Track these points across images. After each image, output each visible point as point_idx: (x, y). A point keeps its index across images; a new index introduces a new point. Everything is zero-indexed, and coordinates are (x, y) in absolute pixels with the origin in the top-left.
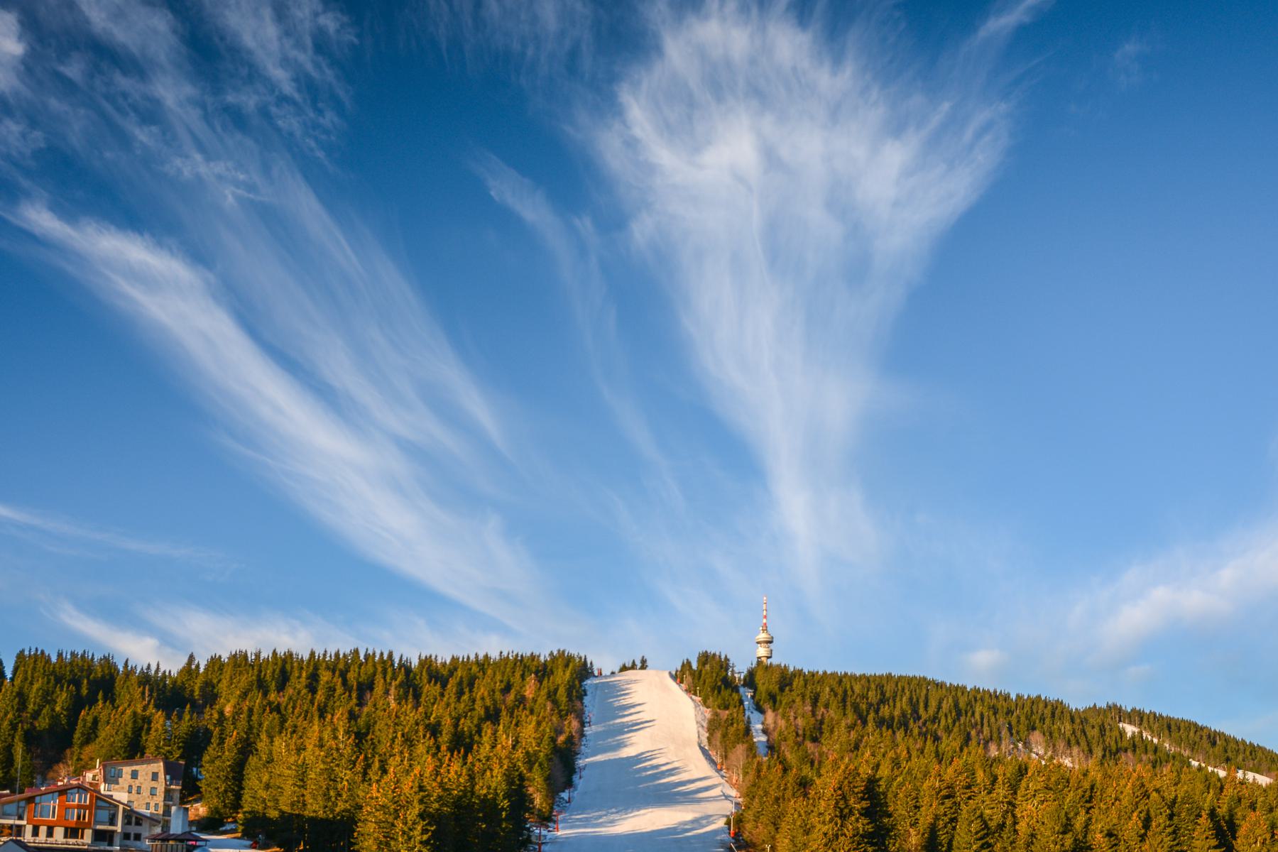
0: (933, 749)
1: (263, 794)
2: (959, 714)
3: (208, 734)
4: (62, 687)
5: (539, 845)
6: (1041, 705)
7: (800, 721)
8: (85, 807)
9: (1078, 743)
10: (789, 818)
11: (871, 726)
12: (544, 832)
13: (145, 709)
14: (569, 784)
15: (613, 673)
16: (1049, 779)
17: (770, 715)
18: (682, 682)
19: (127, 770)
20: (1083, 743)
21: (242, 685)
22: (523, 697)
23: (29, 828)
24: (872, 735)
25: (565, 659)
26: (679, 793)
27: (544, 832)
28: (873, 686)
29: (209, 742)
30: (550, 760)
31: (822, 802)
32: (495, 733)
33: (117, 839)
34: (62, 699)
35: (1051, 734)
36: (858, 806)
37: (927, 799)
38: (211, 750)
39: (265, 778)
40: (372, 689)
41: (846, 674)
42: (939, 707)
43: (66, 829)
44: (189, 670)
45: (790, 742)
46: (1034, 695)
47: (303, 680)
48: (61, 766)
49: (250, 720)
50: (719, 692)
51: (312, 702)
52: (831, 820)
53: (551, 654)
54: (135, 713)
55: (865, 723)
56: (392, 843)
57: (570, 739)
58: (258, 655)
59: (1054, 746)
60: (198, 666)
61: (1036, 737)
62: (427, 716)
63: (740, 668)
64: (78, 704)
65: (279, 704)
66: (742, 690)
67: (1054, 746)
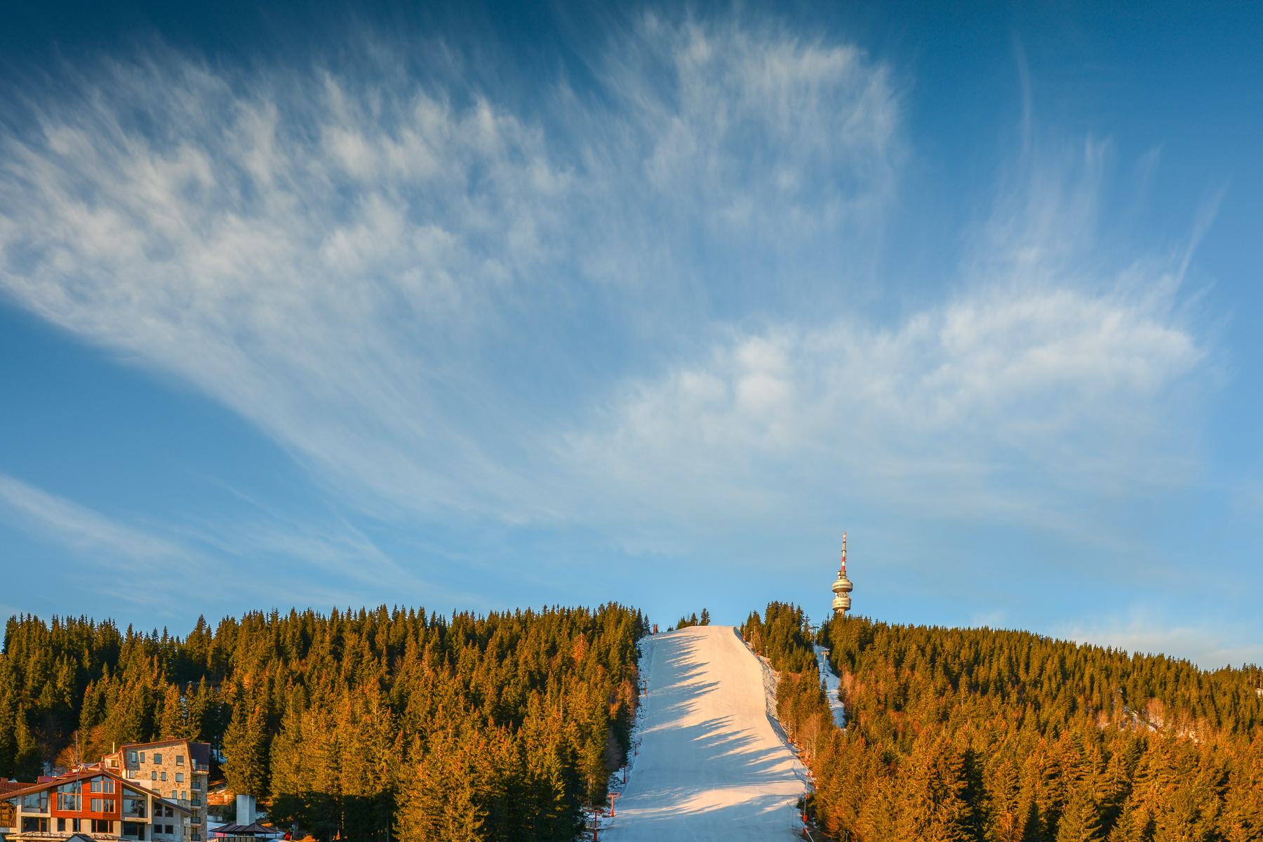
0: (1034, 718)
1: (293, 778)
2: (1065, 676)
3: (227, 710)
4: (62, 659)
5: (595, 832)
6: (1163, 667)
7: (881, 686)
8: (111, 797)
9: (1205, 713)
10: (872, 800)
11: (963, 689)
12: (599, 817)
13: (156, 682)
14: (623, 762)
15: (670, 630)
16: (1173, 756)
17: (848, 677)
18: (748, 640)
19: (149, 753)
20: (1212, 714)
21: (260, 652)
22: (570, 659)
23: (54, 823)
24: (964, 702)
25: (615, 613)
26: (761, 775)
27: (599, 817)
28: (967, 644)
29: (229, 720)
30: (602, 734)
31: (912, 782)
32: (542, 701)
33: (148, 832)
34: (64, 673)
35: (1173, 701)
36: (954, 787)
37: (1028, 779)
38: (233, 729)
39: (295, 760)
40: (403, 654)
41: (936, 628)
42: (1042, 670)
43: (93, 822)
44: (200, 634)
45: (871, 711)
46: (1155, 654)
47: (327, 645)
48: (70, 750)
49: (271, 693)
50: (791, 651)
51: (338, 670)
52: (924, 802)
53: (602, 607)
54: (145, 689)
55: (956, 687)
56: (442, 832)
57: (623, 710)
58: (275, 616)
59: (1176, 716)
60: (209, 631)
61: (1156, 705)
62: (467, 686)
63: (815, 620)
64: (81, 680)
65: (302, 675)
66: (816, 648)
67: (1176, 716)
